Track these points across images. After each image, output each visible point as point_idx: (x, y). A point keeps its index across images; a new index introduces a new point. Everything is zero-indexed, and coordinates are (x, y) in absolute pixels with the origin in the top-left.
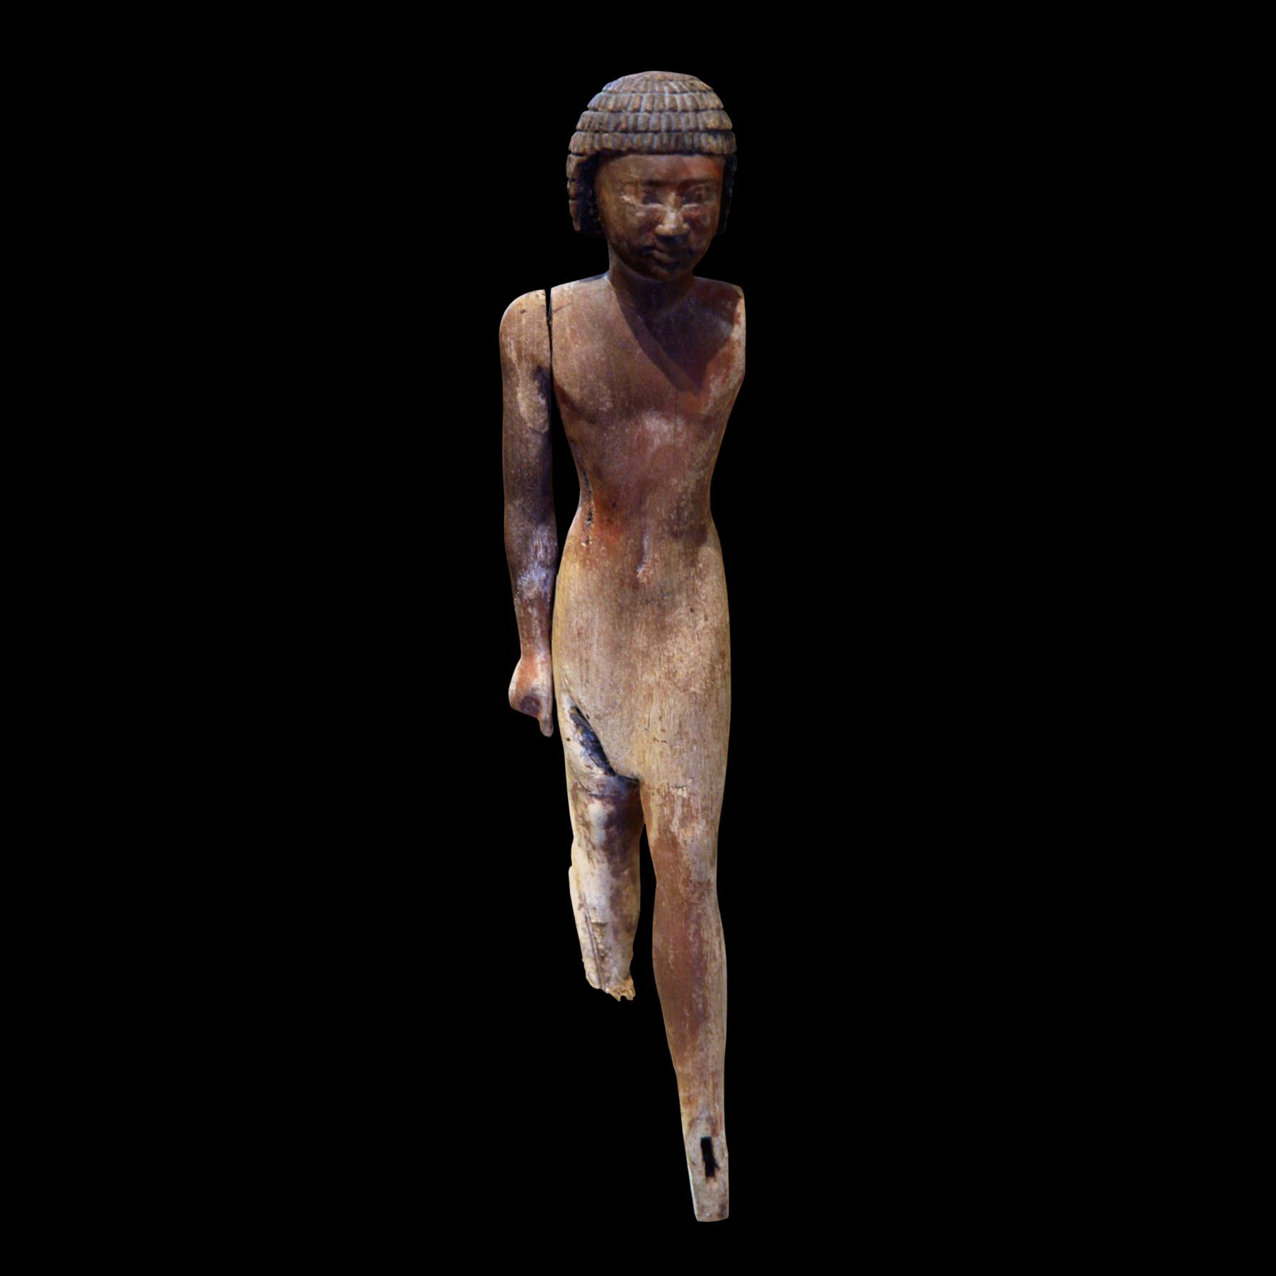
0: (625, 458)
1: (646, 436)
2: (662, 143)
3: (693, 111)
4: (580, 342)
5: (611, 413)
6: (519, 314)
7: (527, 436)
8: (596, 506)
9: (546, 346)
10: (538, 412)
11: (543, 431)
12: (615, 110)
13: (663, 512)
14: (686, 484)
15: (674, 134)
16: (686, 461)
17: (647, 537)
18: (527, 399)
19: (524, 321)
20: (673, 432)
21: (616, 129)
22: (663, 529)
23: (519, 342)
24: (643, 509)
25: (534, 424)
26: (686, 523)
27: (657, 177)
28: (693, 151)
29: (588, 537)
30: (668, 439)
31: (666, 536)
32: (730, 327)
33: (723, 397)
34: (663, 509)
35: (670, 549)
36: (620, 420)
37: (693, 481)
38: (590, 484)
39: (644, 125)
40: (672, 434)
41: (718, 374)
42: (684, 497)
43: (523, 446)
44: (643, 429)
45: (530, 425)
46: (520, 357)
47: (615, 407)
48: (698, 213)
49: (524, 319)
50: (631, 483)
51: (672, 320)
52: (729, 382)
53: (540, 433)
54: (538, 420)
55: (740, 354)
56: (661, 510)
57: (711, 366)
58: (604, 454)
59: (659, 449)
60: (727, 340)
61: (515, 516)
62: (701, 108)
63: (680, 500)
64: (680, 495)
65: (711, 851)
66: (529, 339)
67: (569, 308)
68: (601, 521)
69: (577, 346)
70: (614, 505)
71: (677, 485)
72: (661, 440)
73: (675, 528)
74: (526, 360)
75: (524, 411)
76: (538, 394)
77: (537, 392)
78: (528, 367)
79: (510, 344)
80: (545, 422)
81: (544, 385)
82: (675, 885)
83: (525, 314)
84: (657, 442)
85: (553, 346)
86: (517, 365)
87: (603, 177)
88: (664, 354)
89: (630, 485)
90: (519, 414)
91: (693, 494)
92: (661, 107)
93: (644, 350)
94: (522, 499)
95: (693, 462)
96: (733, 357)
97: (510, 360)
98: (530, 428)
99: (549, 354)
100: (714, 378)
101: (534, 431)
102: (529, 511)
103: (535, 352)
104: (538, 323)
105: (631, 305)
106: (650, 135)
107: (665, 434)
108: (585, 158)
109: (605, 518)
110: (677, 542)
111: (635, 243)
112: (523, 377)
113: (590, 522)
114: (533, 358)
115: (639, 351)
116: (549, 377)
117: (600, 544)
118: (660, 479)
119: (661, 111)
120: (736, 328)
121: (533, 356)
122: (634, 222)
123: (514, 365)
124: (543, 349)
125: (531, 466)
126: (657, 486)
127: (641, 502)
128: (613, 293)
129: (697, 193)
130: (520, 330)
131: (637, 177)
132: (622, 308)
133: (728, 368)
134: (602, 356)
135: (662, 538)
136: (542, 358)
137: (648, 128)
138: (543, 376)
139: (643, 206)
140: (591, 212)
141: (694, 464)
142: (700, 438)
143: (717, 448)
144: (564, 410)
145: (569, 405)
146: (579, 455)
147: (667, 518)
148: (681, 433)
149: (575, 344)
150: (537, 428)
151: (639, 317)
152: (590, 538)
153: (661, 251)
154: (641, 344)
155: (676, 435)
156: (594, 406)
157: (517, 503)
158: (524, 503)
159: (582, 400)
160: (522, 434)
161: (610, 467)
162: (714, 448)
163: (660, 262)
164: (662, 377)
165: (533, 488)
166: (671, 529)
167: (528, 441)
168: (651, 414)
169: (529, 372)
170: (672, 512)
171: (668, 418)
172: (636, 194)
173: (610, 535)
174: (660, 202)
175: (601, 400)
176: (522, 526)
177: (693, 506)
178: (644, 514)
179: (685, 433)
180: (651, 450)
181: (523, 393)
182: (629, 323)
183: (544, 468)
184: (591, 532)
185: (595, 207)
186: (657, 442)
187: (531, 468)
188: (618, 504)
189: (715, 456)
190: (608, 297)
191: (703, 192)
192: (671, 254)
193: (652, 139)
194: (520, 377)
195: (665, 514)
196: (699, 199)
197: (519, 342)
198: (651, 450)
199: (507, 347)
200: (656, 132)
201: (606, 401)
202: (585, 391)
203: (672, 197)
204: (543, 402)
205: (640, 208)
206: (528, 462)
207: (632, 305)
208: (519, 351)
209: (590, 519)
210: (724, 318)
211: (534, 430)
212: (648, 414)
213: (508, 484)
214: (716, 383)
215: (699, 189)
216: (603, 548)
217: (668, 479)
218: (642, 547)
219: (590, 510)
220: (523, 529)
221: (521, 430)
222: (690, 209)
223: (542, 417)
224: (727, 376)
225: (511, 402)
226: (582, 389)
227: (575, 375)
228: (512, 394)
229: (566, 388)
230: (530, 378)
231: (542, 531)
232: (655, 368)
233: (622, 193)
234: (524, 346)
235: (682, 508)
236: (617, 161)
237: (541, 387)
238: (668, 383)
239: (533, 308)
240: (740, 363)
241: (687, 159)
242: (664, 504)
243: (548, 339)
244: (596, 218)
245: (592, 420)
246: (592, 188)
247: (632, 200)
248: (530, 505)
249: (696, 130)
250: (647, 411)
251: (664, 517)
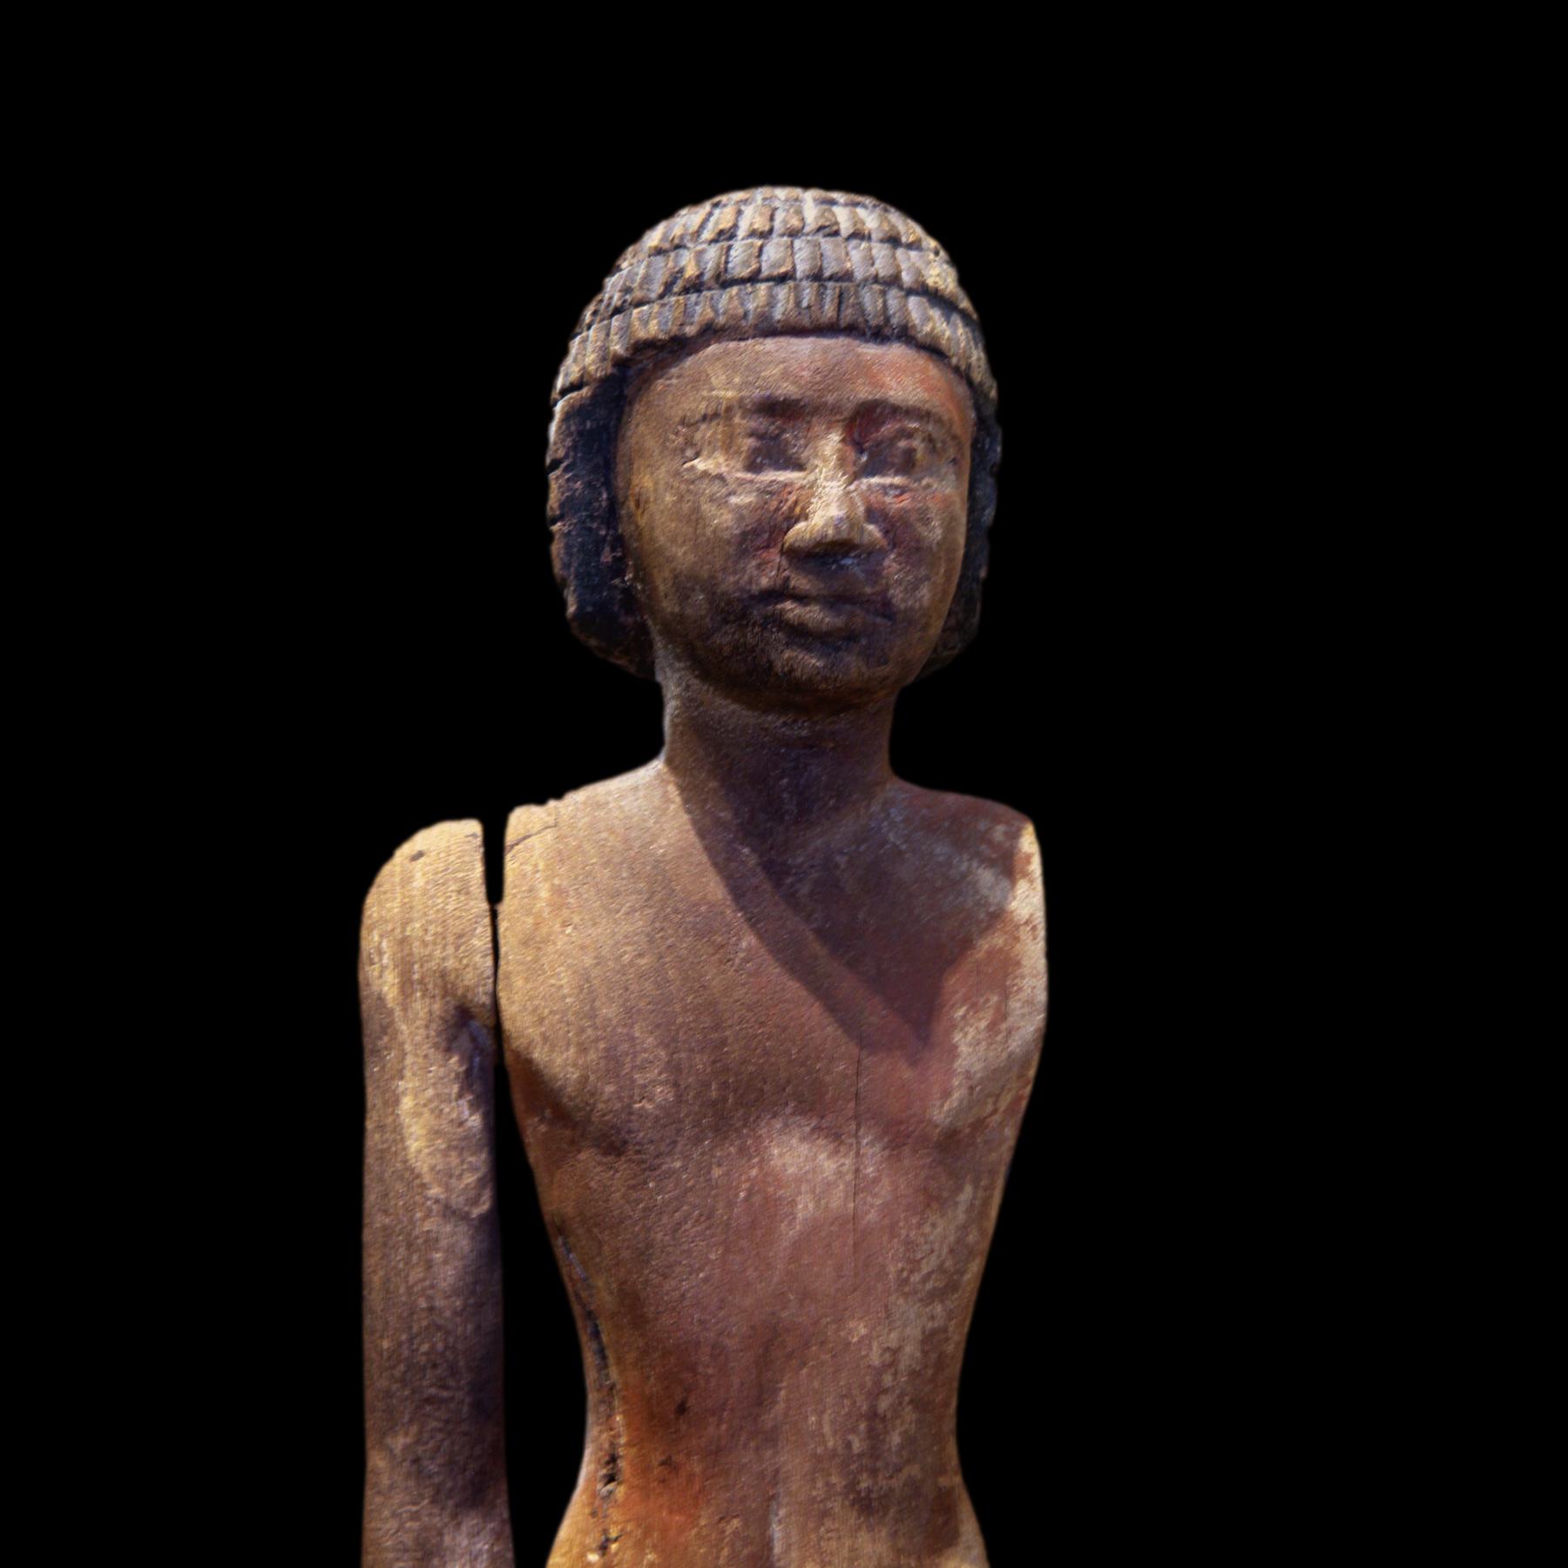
0: (713, 1257)
1: (771, 1190)
2: (798, 303)
3: (882, 241)
4: (576, 919)
5: (668, 1118)
6: (406, 862)
7: (427, 1226)
8: (628, 1425)
9: (482, 941)
10: (461, 1151)
11: (476, 1212)
12: (666, 245)
13: (827, 1429)
14: (893, 1339)
15: (830, 284)
16: (892, 1269)
17: (782, 1512)
18: (427, 1115)
19: (419, 882)
20: (849, 1177)
21: (668, 288)
22: (827, 1484)
23: (403, 941)
24: (769, 1419)
25: (448, 1189)
26: (899, 1470)
27: (787, 390)
28: (887, 331)
29: (605, 1531)
30: (837, 1199)
31: (836, 1505)
32: (1005, 883)
34: (826, 1417)
35: (852, 1550)
36: (697, 1141)
37: (914, 1332)
38: (611, 1360)
39: (746, 263)
40: (847, 1184)
41: (974, 1007)
42: (888, 1380)
43: (415, 1258)
44: (761, 1169)
45: (435, 1191)
46: (406, 986)
47: (679, 1099)
48: (906, 502)
49: (418, 875)
50: (730, 1336)
51: (842, 860)
52: (1009, 1032)
53: (465, 1217)
54: (460, 1177)
55: (1033, 953)
56: (820, 1423)
57: (955, 983)
58: (650, 1245)
59: (813, 1228)
60: (997, 917)
61: (391, 1487)
63: (879, 1391)
64: (879, 1372)
66: (432, 929)
67: (549, 836)
68: (643, 1470)
69: (569, 930)
70: (682, 1409)
71: (866, 1340)
72: (818, 1202)
73: (865, 1483)
74: (425, 992)
75: (419, 1151)
76: (460, 1096)
77: (455, 1089)
78: (430, 1013)
79: (380, 953)
80: (481, 1182)
81: (475, 1071)
82: (803, 382)
83: (422, 860)
84: (805, 1207)
85: (502, 941)
86: (398, 1013)
87: (640, 431)
88: (818, 948)
89: (727, 1342)
90: (405, 1162)
91: (914, 1374)
92: (795, 222)
93: (760, 936)
94: (414, 1429)
95: (911, 1272)
96: (1018, 964)
97: (381, 998)
98: (437, 1201)
99: (489, 962)
100: (964, 1017)
101: (448, 1212)
102: (433, 1468)
103: (450, 964)
104: (456, 880)
105: (775, 1507)
106: (763, 288)
107: (829, 1185)
108: (585, 391)
109: (657, 1458)
110: (871, 1529)
111: (729, 582)
112: (417, 1045)
113: (610, 1487)
114: (445, 983)
115: (749, 940)
116: (488, 1042)
117: (640, 1546)
118: (816, 1323)
119: (793, 233)
120: (1022, 887)
121: (443, 974)
122: (722, 520)
123: (391, 1012)
124: (471, 952)
125: (440, 1322)
126: (807, 1345)
127: (761, 1396)
128: (673, 791)
129: (902, 444)
130: (407, 907)
131: (730, 394)
132: (694, 822)
133: (1005, 995)
134: (641, 955)
135: (826, 1514)
136: (469, 978)
138: (474, 1039)
139: (749, 476)
140: (607, 557)
141: (915, 1278)
142: (931, 1200)
143: (980, 1239)
144: (534, 1130)
145: (548, 1112)
146: (578, 1271)
147: (840, 1450)
148: (876, 1181)
149: (565, 924)
150: (457, 1201)
151: (746, 851)
153: (802, 599)
154: (753, 922)
155: (860, 1186)
156: (620, 1099)
157: (399, 1442)
158: (417, 1442)
159: (584, 1080)
160: (412, 1221)
161: (669, 1285)
162: (972, 1238)
163: (800, 634)
164: (813, 1012)
165: (445, 1394)
166: (852, 1486)
167: (431, 1241)
168: (786, 1125)
169: (434, 1026)
170: (854, 1430)
171: (836, 1137)
172: (728, 446)
173: (671, 1512)
174: (800, 467)
175: (639, 1078)
176: (415, 1516)
177: (914, 1416)
178: (770, 1438)
179: (885, 1181)
180: (789, 1233)
181: (416, 1093)
182: (715, 865)
183: (478, 1328)
184: (615, 1514)
185: (619, 542)
186: (805, 1207)
187: (439, 1328)
188: (691, 1402)
189: (975, 1268)
190: (657, 801)
193: (771, 302)
194: (408, 1047)
195: (835, 1432)
196: (907, 465)
197: (403, 941)
198: (789, 1233)
200: (782, 279)
201: (654, 1082)
202: (592, 1056)
203: (831, 443)
204: (475, 1121)
205: (741, 482)
206: (431, 1309)
207: (726, 815)
208: (405, 968)
210: (990, 863)
211: (447, 1207)
212: (778, 1125)
213: (378, 1381)
214: (971, 1032)
215: (909, 435)
216: (651, 1557)
217: (839, 1321)
218: (768, 1545)
219: (612, 1444)
220: (415, 1525)
221: (409, 1209)
222: (884, 489)
223: (473, 1169)
224: (1002, 1015)
226: (583, 1049)
227: (564, 1013)
228: (386, 1103)
229: (539, 1055)
230: (436, 1046)
231: (473, 1535)
232: (793, 987)
233: (689, 453)
234: (417, 949)
235: (883, 1419)
236: (674, 371)
237: (468, 1073)
238: (832, 1030)
240: (1033, 982)
241: (870, 350)
242: (829, 1400)
243: (487, 921)
244: (620, 573)
245: (613, 1144)
246: (608, 484)
247: (718, 465)
248: (437, 1449)
249: (894, 281)
250: (775, 1116)
251: (830, 1444)
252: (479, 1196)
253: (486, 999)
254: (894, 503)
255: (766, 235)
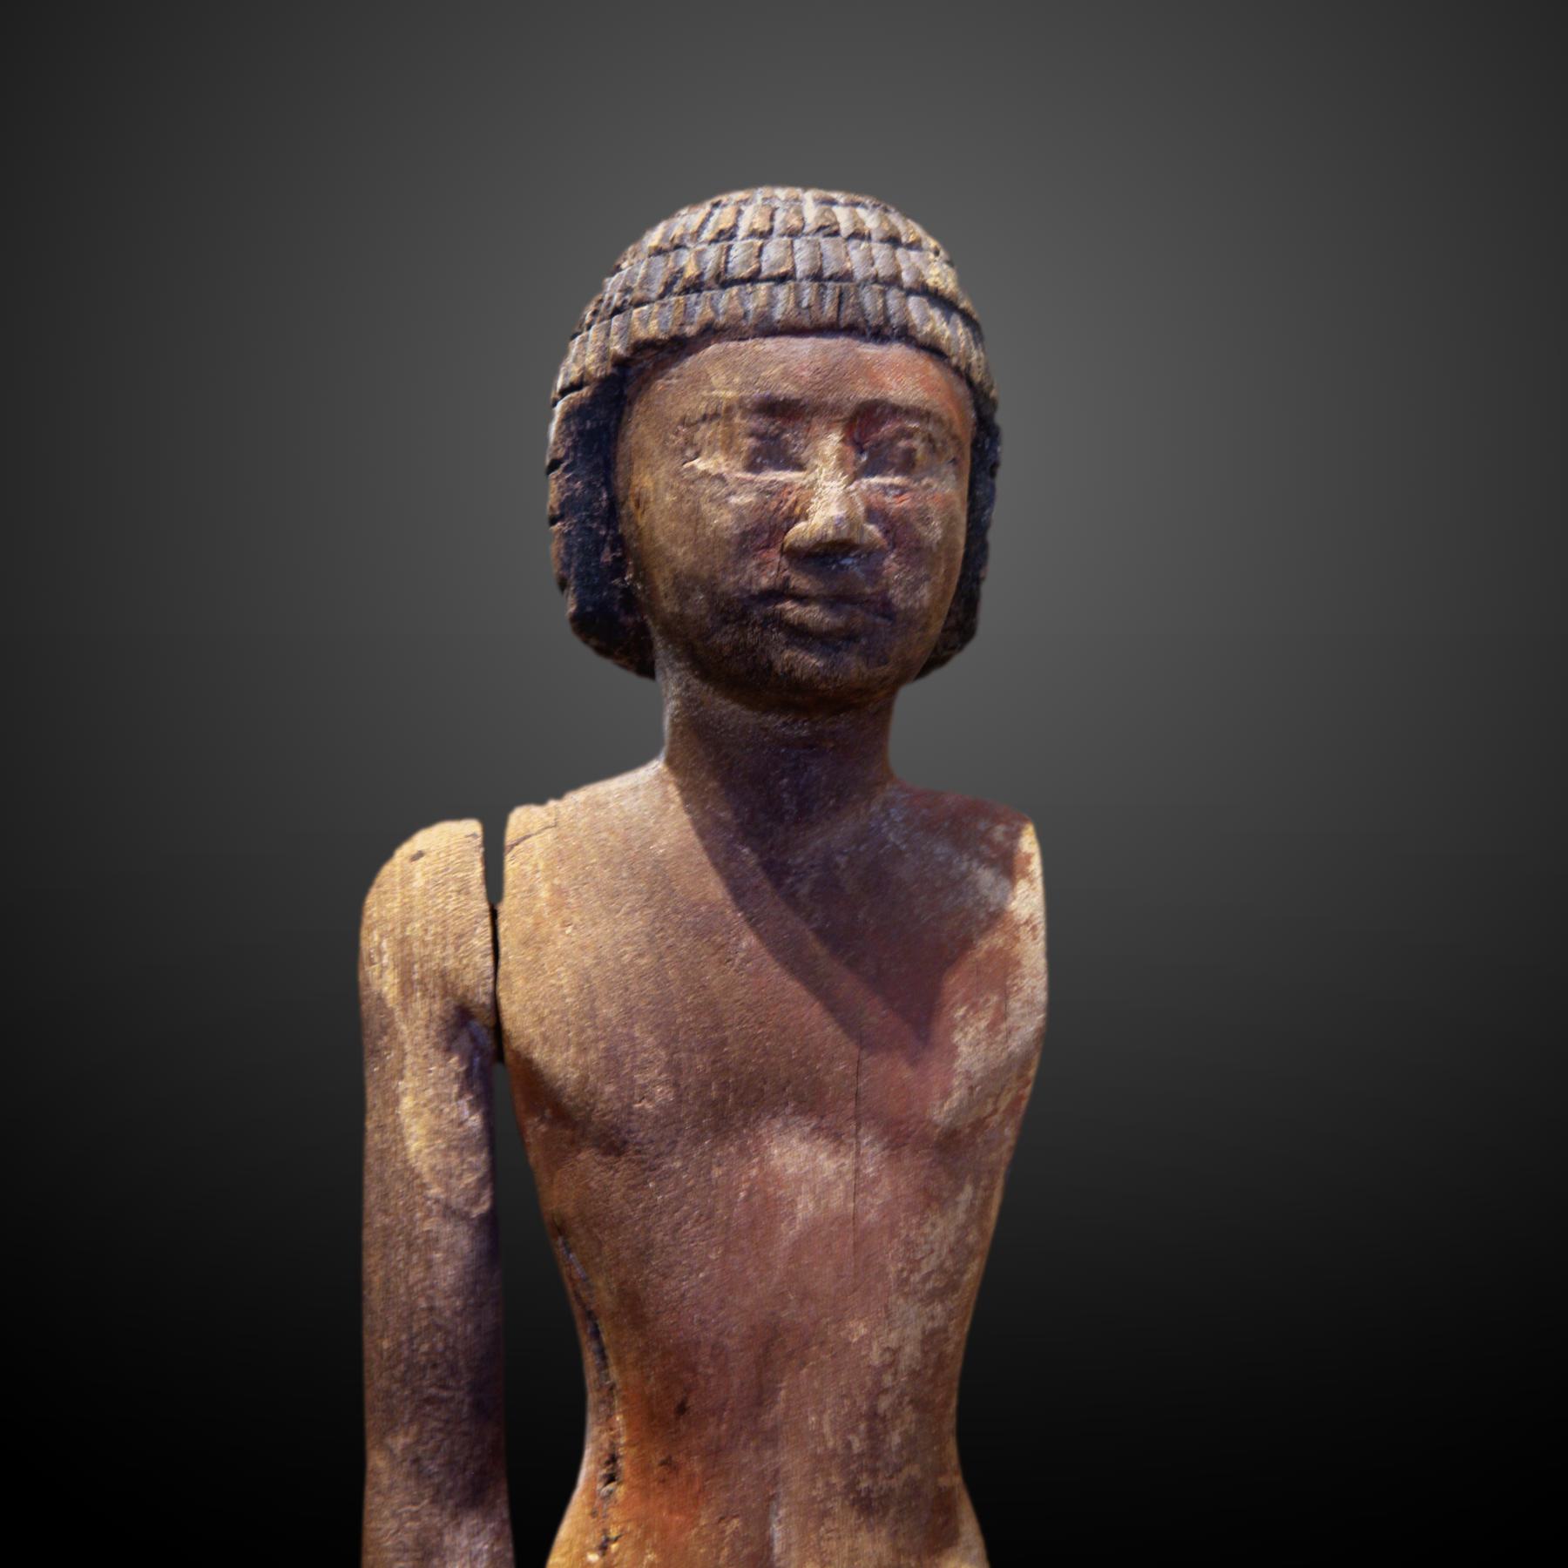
0: (713, 1257)
1: (771, 1190)
2: (798, 303)
5: (668, 1118)
6: (406, 862)
7: (427, 1226)
8: (628, 1425)
9: (482, 941)
10: (461, 1151)
11: (476, 1212)
12: (666, 245)
13: (827, 1429)
14: (893, 1339)
15: (830, 284)
16: (892, 1269)
17: (782, 1512)
18: (427, 1115)
19: (419, 882)
20: (849, 1177)
21: (668, 288)
22: (827, 1484)
23: (403, 941)
24: (769, 1419)
25: (448, 1189)
26: (899, 1470)
27: (787, 390)
28: (887, 331)
29: (605, 1531)
30: (837, 1199)
31: (836, 1505)
32: (1005, 883)
33: (995, 1077)
34: (826, 1417)
35: (852, 1550)
36: (697, 1141)
37: (914, 1332)
38: (611, 1360)
39: (746, 263)
40: (847, 1184)
41: (974, 1007)
42: (888, 1380)
43: (415, 1258)
45: (435, 1191)
46: (406, 986)
47: (679, 1099)
48: (906, 502)
49: (418, 875)
50: (730, 1336)
51: (842, 860)
52: (1009, 1032)
53: (465, 1217)
54: (460, 1177)
55: (1033, 953)
56: (820, 1423)
57: (955, 983)
58: (650, 1245)
59: (813, 1228)
60: (997, 917)
61: (391, 1487)
62: (904, 239)
63: (879, 1391)
64: (879, 1372)
65: (931, 366)
66: (432, 929)
67: (549, 836)
68: (643, 1470)
69: (569, 930)
70: (682, 1409)
71: (866, 1340)
72: (818, 1202)
73: (865, 1483)
74: (425, 992)
75: (419, 1151)
76: (460, 1096)
77: (455, 1089)
78: (430, 1013)
79: (380, 953)
80: (481, 1183)
81: (475, 1071)
83: (422, 860)
84: (805, 1207)
85: (502, 941)
86: (398, 1013)
87: (640, 431)
88: (818, 948)
89: (727, 1342)
90: (405, 1162)
91: (914, 1374)
92: (795, 222)
93: (760, 936)
94: (414, 1429)
96: (1018, 964)
97: (381, 998)
98: (437, 1201)
99: (489, 962)
100: (964, 1017)
101: (448, 1212)
102: (433, 1468)
103: (450, 964)
104: (456, 880)
105: (775, 1507)
106: (763, 288)
107: (829, 1185)
108: (585, 391)
109: (657, 1458)
110: (871, 1529)
111: (729, 582)
112: (417, 1045)
114: (445, 983)
115: (749, 940)
116: (488, 1042)
117: (640, 1546)
118: (816, 1323)
119: (793, 233)
120: (1022, 887)
121: (443, 974)
122: (722, 520)
123: (391, 1012)
124: (471, 952)
125: (440, 1322)
126: (807, 1345)
127: (761, 1396)
128: (673, 791)
129: (902, 444)
130: (407, 907)
131: (730, 394)
132: (694, 822)
133: (1005, 995)
134: (641, 955)
135: (826, 1514)
136: (469, 978)
137: (759, 271)
138: (474, 1039)
139: (749, 476)
140: (607, 557)
141: (915, 1278)
142: (931, 1200)
145: (548, 1112)
147: (840, 1450)
148: (876, 1181)
149: (565, 924)
150: (457, 1201)
151: (746, 851)
152: (613, 1534)
153: (802, 599)
154: (753, 922)
155: (860, 1186)
157: (399, 1442)
158: (417, 1442)
159: (584, 1080)
160: (412, 1221)
161: (669, 1285)
162: (972, 1238)
163: (800, 634)
164: (813, 1012)
165: (445, 1394)
166: (852, 1486)
167: (431, 1241)
168: (786, 1125)
169: (434, 1026)
170: (854, 1430)
172: (728, 446)
173: (671, 1512)
174: (800, 467)
175: (639, 1078)
176: (415, 1516)
177: (914, 1416)
178: (770, 1438)
179: (885, 1181)
180: (789, 1233)
181: (416, 1093)
182: (715, 865)
183: (478, 1328)
184: (615, 1514)
185: (619, 542)
186: (805, 1207)
187: (439, 1328)
188: (691, 1402)
190: (657, 801)
191: (917, 443)
192: (834, 601)
193: (771, 302)
194: (408, 1047)
195: (835, 1432)
196: (907, 465)
197: (403, 941)
198: (789, 1233)
199: (372, 963)
200: (782, 279)
201: (654, 1082)
202: (592, 1056)
203: (831, 443)
204: (475, 1121)
205: (741, 482)
206: (431, 1309)
207: (726, 815)
208: (405, 968)
209: (611, 1479)
210: (990, 863)
211: (447, 1207)
212: (778, 1125)
213: (378, 1382)
214: (971, 1032)
215: (909, 435)
216: (651, 1557)
217: (839, 1321)
218: (768, 1545)
219: (612, 1444)
220: (415, 1525)
221: (409, 1209)
222: (884, 489)
223: (473, 1169)
224: (1002, 1015)
225: (381, 1128)
226: (583, 1049)
227: (564, 1013)
228: (386, 1103)
229: (539, 1055)
230: (436, 1046)
231: (473, 1535)
232: (793, 987)
233: (689, 453)
234: (417, 949)
235: (883, 1419)
237: (468, 1073)
238: (832, 1030)
239: (443, 844)
241: (870, 350)
242: (829, 1400)
243: (487, 921)
245: (613, 1144)
246: (608, 484)
247: (718, 465)
248: (437, 1449)
249: (894, 281)
250: (775, 1116)
251: (830, 1444)
252: (479, 1196)
253: (486, 999)
254: (894, 503)
255: (766, 235)
